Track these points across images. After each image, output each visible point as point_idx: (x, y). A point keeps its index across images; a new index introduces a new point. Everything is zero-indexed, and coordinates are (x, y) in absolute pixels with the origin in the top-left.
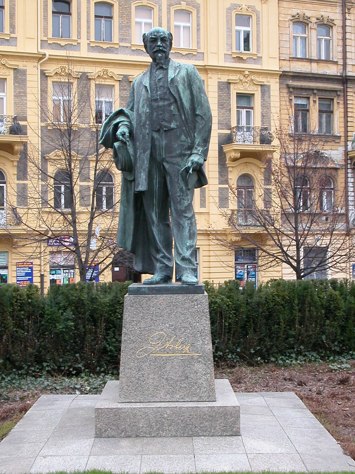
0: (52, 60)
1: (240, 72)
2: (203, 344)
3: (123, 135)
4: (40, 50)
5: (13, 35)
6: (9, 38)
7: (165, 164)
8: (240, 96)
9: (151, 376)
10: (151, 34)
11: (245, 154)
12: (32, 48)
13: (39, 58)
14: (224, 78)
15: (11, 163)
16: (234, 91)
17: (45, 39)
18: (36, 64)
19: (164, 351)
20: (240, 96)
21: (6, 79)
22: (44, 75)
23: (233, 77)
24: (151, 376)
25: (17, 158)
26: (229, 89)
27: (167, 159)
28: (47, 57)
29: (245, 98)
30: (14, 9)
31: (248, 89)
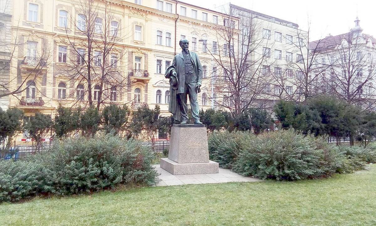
0: (59, 36)
1: (137, 48)
2: (205, 144)
3: (175, 74)
4: (54, 31)
5: (41, 24)
6: (40, 25)
7: (189, 85)
8: (136, 58)
9: (189, 154)
10: (184, 41)
11: (139, 80)
12: (50, 30)
13: (54, 35)
14: (131, 50)
15: (40, 78)
16: (134, 55)
17: (56, 27)
18: (52, 37)
19: (193, 146)
20: (136, 58)
21: (38, 42)
22: (55, 42)
23: (134, 50)
24: (189, 154)
25: (42, 76)
26: (132, 54)
27: (190, 83)
28: (57, 35)
29: (139, 59)
30: (42, 12)
31: (141, 55)
